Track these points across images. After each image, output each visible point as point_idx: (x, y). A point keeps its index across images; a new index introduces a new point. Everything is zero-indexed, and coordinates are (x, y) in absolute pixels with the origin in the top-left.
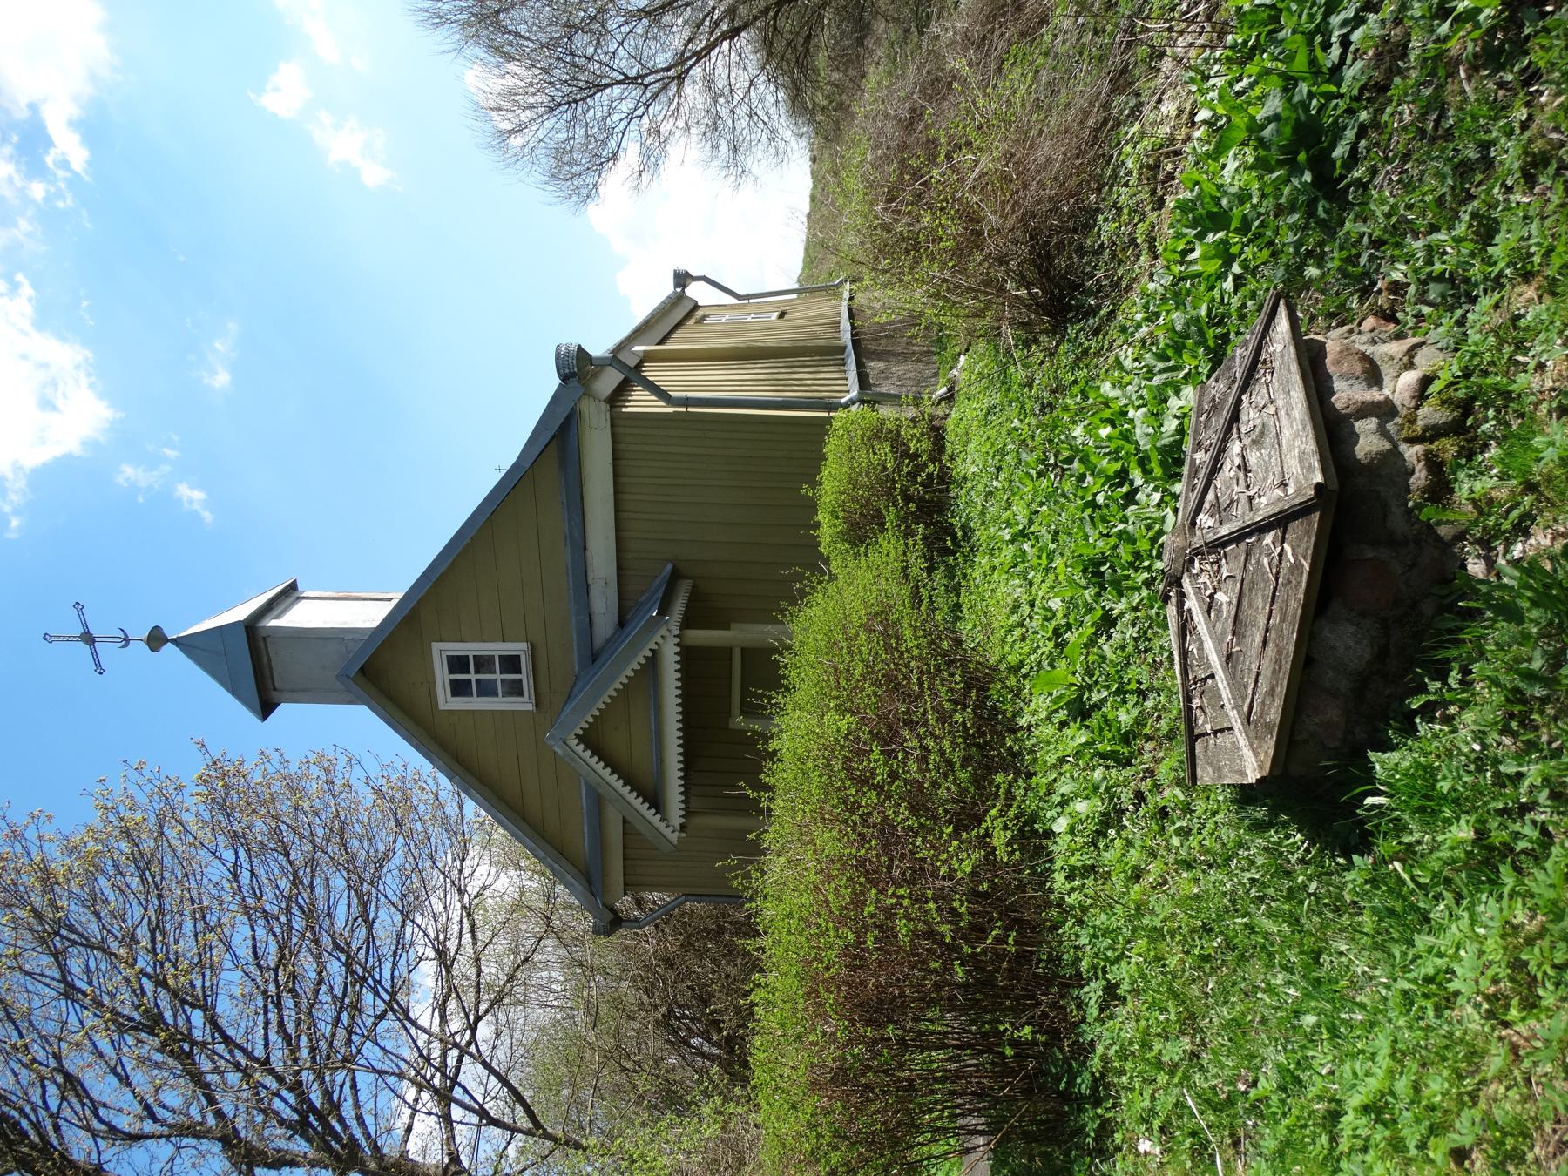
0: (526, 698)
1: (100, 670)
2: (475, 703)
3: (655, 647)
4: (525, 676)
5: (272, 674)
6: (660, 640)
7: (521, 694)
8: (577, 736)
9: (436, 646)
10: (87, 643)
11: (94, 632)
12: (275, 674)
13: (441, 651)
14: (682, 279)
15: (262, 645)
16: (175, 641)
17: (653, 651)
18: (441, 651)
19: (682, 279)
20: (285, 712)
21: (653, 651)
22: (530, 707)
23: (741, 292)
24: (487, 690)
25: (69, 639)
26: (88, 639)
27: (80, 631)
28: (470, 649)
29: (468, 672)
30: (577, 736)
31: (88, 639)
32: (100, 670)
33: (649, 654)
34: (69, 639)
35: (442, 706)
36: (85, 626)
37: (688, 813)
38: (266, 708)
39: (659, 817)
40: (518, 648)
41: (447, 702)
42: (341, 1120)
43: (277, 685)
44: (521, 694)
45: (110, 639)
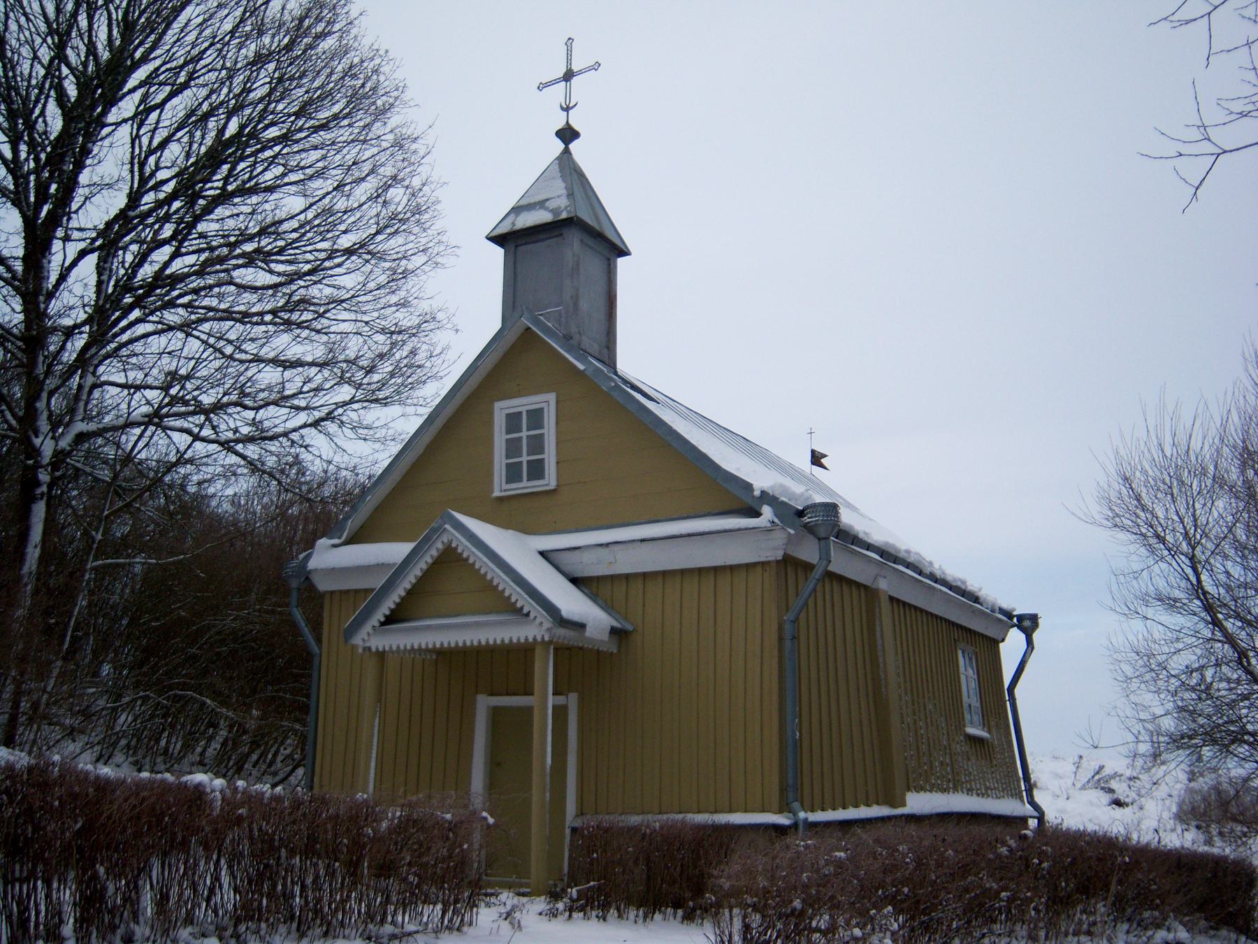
0: (505, 486)
1: (542, 87)
2: (500, 438)
3: (532, 615)
4: (526, 486)
5: (533, 242)
6: (538, 621)
7: (509, 481)
8: (450, 542)
9: (551, 397)
10: (565, 74)
11: (575, 80)
12: (532, 245)
13: (547, 402)
14: (1028, 624)
15: (556, 233)
16: (566, 151)
17: (528, 614)
18: (547, 402)
19: (1028, 624)
20: (499, 252)
21: (528, 614)
22: (497, 493)
23: (1017, 691)
24: (537, 444)
25: (569, 60)
26: (569, 76)
27: (575, 68)
28: (549, 431)
29: (528, 430)
30: (450, 542)
31: (569, 76)
32: (542, 87)
33: (525, 611)
34: (569, 60)
35: (498, 405)
36: (580, 72)
37: (381, 655)
38: (498, 240)
39: (377, 624)
40: (550, 479)
41: (502, 409)
42: (138, 321)
43: (520, 249)
44: (509, 481)
45: (568, 95)
